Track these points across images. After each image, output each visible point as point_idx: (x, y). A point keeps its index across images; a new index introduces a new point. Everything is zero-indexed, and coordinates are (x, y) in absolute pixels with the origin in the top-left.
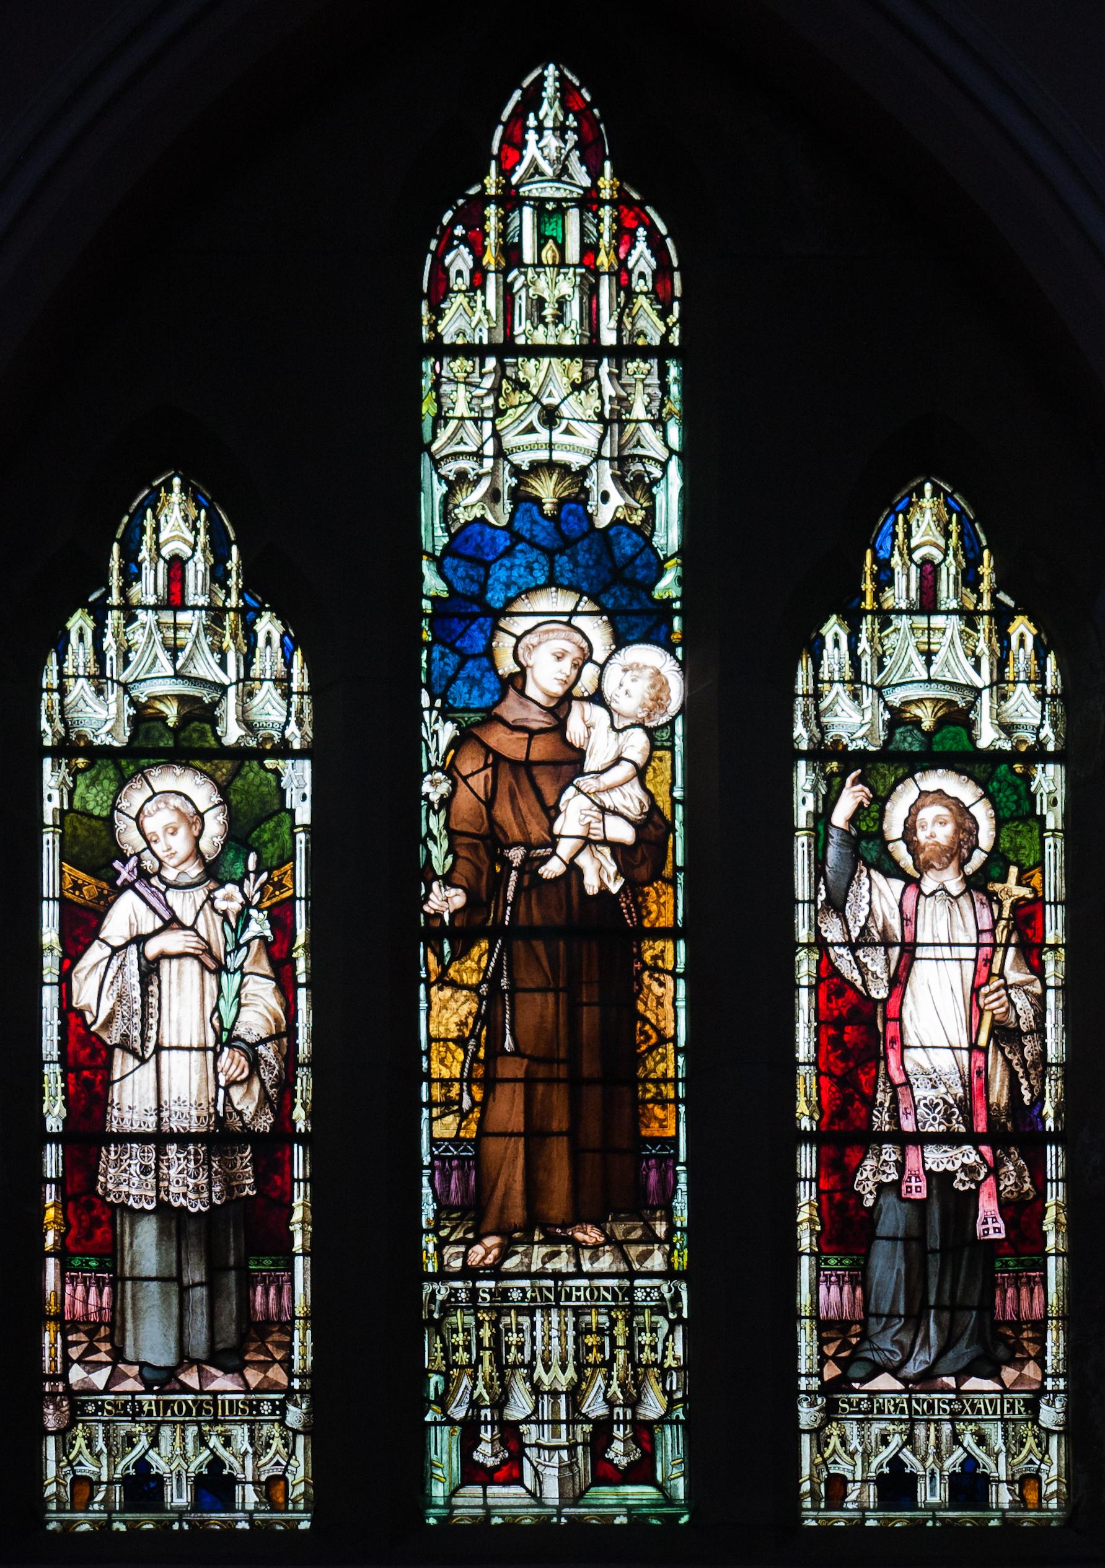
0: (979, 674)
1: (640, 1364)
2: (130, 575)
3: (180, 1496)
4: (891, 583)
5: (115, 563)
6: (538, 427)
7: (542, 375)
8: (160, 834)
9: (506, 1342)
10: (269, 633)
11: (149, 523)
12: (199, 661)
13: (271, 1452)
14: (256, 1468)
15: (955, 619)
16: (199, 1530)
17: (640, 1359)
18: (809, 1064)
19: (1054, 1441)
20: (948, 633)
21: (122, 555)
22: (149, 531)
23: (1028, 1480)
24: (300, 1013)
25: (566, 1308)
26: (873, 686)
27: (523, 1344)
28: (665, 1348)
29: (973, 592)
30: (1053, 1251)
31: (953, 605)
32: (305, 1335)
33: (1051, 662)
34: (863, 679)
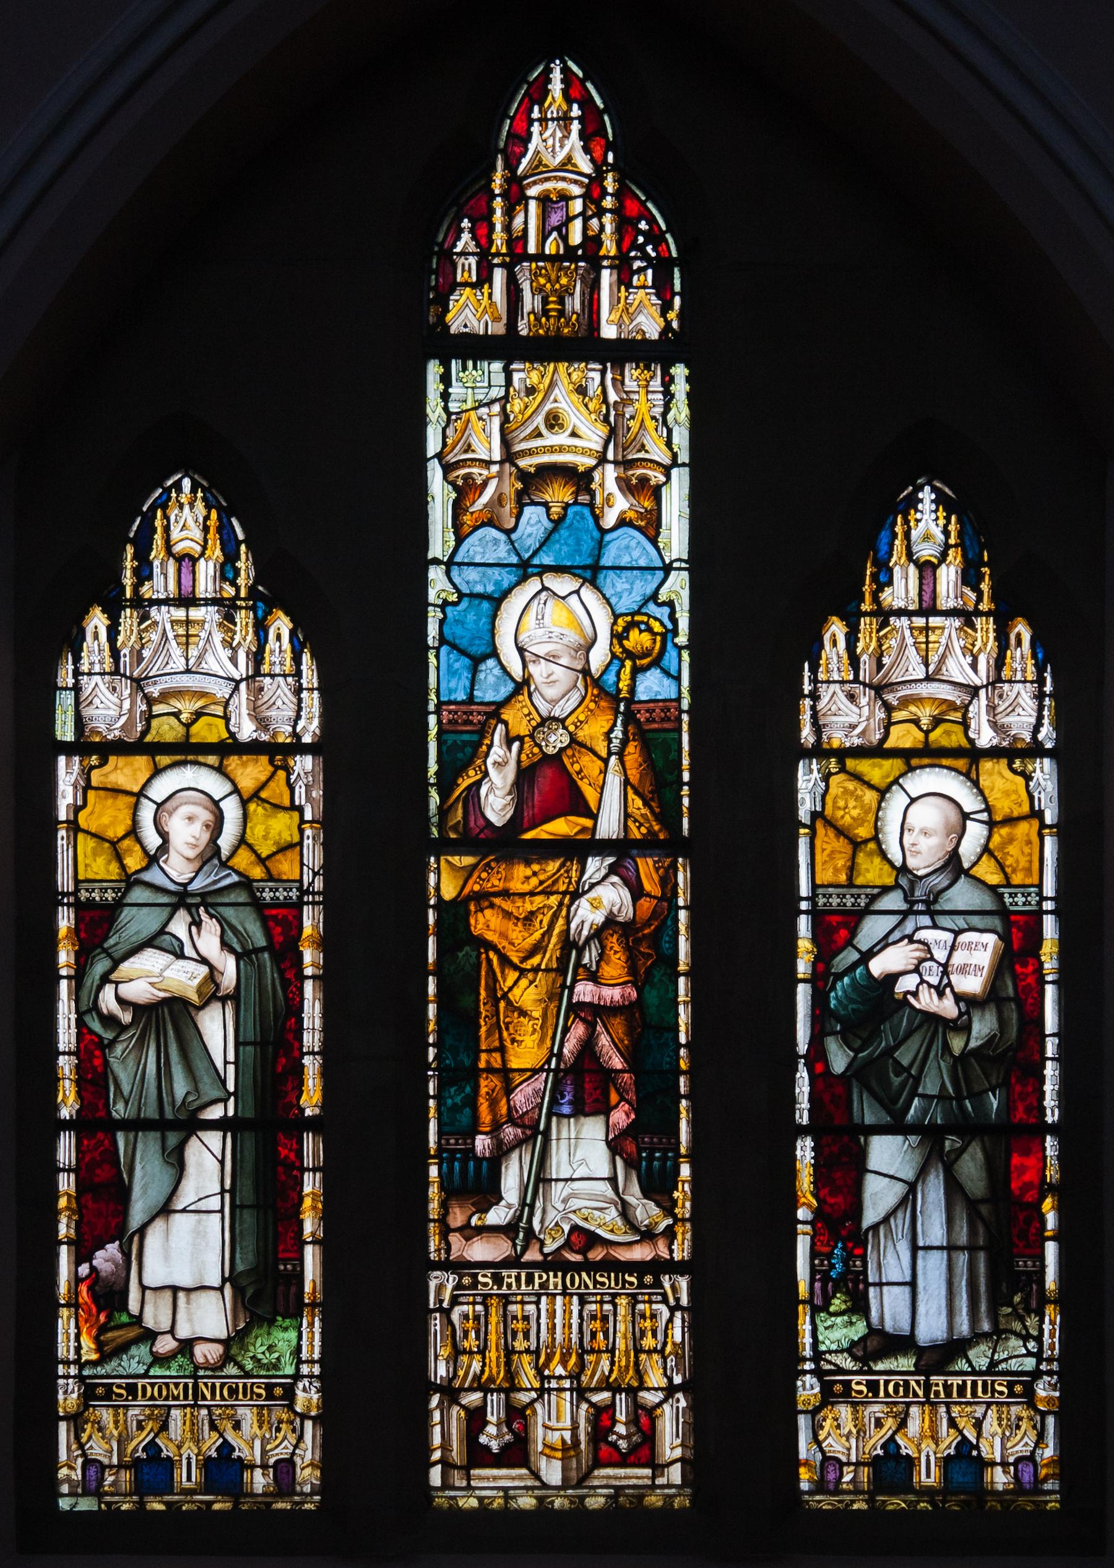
0: (236, 667)
1: (514, 1352)
2: (143, 574)
3: (928, 1476)
4: (150, 577)
5: (129, 564)
6: (544, 431)
7: (547, 381)
8: (917, 830)
9: (513, 1329)
10: (96, 627)
11: (158, 523)
12: (209, 658)
13: (1020, 1434)
14: (264, 1452)
15: (212, 609)
16: (876, 1511)
17: (513, 1346)
18: (69, 1053)
19: (309, 1424)
20: (207, 626)
21: (135, 557)
22: (159, 530)
23: (285, 1469)
24: (306, 1002)
25: (571, 1295)
26: (131, 678)
27: (528, 1330)
28: (666, 1336)
29: (973, 590)
30: (310, 1239)
31: (951, 604)
32: (69, 1324)
33: (306, 658)
34: (861, 678)
